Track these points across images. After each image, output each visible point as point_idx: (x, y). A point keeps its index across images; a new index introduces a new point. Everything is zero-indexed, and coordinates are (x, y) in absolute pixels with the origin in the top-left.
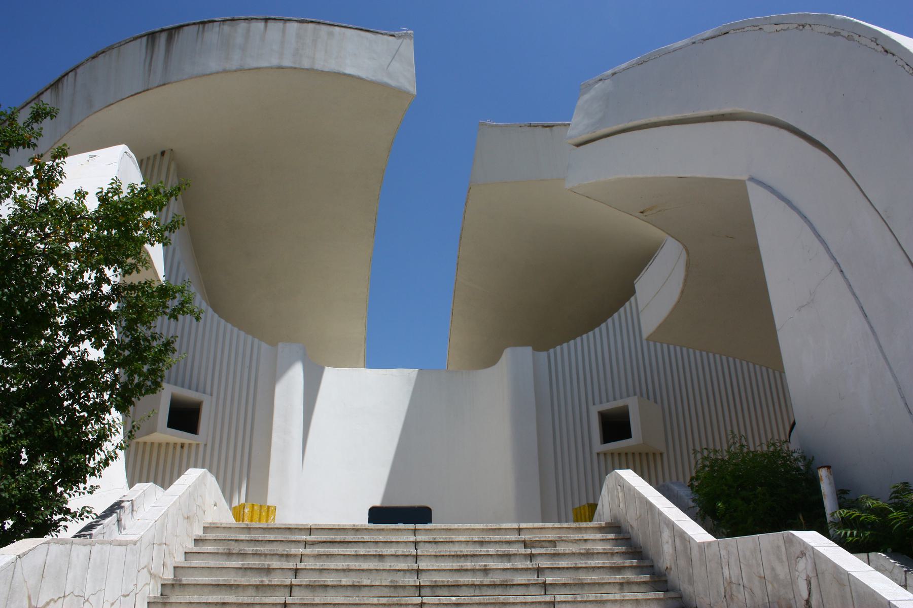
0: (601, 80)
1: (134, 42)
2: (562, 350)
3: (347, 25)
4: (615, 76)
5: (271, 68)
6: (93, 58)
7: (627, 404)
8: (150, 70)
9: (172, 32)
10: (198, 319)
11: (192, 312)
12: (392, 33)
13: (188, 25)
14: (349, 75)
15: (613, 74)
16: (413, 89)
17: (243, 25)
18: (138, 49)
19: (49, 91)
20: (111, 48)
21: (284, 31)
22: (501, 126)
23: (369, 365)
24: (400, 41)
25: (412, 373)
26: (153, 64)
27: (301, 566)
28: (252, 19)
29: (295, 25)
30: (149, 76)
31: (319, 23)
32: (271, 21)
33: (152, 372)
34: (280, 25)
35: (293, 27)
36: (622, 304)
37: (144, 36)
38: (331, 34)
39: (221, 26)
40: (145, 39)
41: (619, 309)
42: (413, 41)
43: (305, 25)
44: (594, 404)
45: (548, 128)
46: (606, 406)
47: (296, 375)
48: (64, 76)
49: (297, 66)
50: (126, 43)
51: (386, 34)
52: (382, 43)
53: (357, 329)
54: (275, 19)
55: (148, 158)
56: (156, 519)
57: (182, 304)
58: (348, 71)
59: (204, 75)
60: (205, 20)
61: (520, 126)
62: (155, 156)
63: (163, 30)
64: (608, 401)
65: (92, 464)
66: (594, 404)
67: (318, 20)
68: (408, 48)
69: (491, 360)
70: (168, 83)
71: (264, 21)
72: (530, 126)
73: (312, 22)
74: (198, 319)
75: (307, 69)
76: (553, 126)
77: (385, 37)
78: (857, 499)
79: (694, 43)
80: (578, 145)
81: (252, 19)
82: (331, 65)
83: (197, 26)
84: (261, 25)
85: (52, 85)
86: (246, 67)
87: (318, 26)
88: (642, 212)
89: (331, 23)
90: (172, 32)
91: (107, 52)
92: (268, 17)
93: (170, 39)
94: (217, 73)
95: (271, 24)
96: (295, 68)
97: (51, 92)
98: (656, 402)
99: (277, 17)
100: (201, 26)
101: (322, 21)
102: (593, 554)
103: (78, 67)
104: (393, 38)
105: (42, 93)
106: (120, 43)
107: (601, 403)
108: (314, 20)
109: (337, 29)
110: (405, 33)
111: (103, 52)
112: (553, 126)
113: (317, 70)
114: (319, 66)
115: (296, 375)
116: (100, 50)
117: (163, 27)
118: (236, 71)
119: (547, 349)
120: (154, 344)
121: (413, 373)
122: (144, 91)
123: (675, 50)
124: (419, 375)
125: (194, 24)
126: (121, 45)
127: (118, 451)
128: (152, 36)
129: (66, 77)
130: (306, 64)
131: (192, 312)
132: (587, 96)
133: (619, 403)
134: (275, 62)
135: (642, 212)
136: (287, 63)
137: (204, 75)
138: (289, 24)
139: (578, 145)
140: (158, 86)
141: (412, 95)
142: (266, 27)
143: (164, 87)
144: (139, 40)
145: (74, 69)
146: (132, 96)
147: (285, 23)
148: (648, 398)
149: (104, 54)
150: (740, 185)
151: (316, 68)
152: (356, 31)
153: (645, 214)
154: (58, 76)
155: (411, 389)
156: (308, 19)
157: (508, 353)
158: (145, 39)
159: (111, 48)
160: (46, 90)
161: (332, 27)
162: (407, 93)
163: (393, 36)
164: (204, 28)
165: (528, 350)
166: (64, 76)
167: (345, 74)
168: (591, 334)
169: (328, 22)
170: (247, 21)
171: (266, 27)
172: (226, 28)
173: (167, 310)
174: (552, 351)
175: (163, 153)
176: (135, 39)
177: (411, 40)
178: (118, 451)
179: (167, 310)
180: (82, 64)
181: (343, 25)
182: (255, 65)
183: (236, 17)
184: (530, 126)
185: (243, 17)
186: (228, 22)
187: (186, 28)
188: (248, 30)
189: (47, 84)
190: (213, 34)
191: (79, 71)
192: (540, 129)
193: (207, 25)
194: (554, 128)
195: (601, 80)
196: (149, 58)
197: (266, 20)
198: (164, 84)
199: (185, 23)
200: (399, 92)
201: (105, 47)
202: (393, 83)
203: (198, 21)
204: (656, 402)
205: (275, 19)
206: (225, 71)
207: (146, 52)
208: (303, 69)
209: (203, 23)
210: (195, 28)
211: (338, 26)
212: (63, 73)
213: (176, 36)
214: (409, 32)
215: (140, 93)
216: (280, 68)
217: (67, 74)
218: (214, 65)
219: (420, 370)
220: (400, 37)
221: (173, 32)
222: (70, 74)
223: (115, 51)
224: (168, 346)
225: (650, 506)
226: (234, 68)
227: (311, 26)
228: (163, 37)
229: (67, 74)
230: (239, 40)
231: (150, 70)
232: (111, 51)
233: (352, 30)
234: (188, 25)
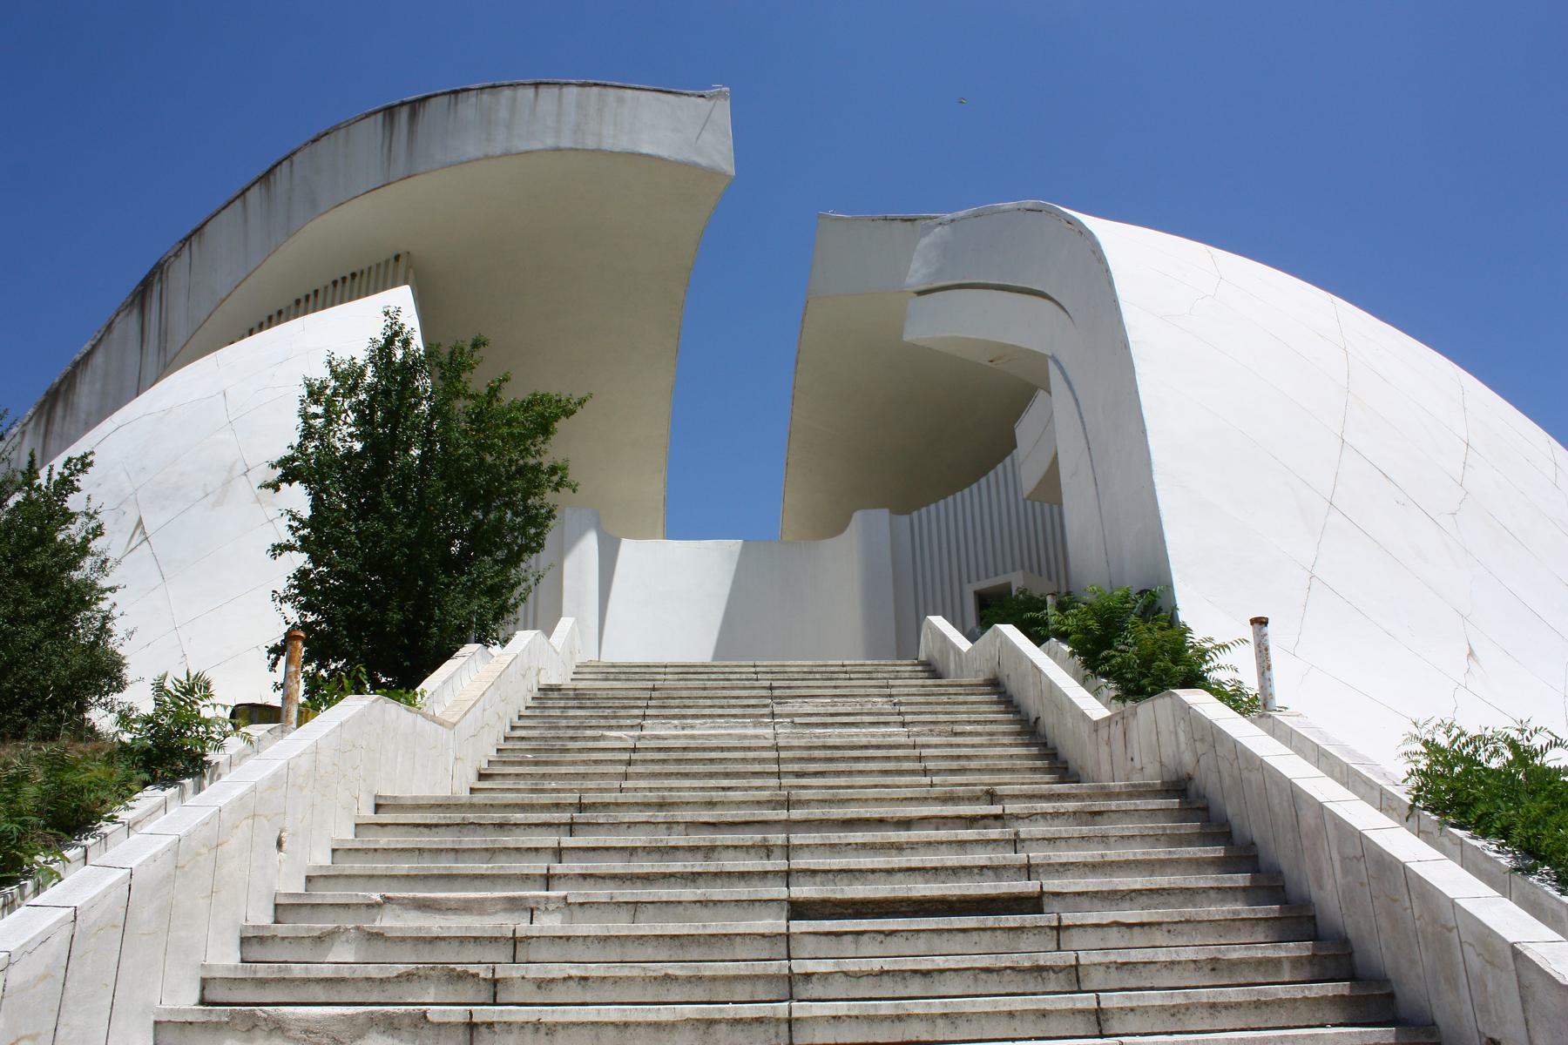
0: (940, 224)
1: (367, 120)
2: (920, 517)
3: (642, 86)
4: (954, 223)
5: (546, 150)
6: (314, 141)
7: (1009, 581)
8: (389, 159)
9: (416, 105)
10: (574, 491)
11: (569, 486)
12: (701, 92)
13: (436, 95)
14: (647, 155)
15: (953, 220)
16: (730, 169)
17: (507, 93)
18: (375, 125)
19: (257, 186)
20: (337, 128)
21: (560, 100)
22: (847, 219)
23: (668, 537)
24: (712, 102)
25: (733, 546)
26: (392, 149)
27: (558, 869)
28: (518, 85)
29: (574, 90)
30: (390, 165)
31: (605, 86)
32: (543, 86)
33: (537, 535)
34: (555, 90)
35: (572, 93)
36: (1001, 459)
37: (379, 111)
38: (621, 100)
39: (479, 96)
40: (380, 116)
41: (1004, 458)
42: (729, 101)
43: (587, 89)
44: (969, 582)
45: (909, 223)
46: (985, 584)
47: (589, 545)
48: (276, 166)
49: (578, 146)
50: (356, 121)
51: (693, 95)
52: (687, 109)
53: (653, 488)
54: (547, 84)
55: (378, 265)
56: (4, 1000)
57: (561, 478)
58: (645, 150)
59: (460, 163)
60: (458, 88)
61: (873, 220)
62: (387, 262)
63: (403, 104)
64: (987, 577)
65: (512, 601)
66: (969, 582)
67: (603, 82)
68: (722, 111)
69: (838, 527)
70: (415, 175)
71: (533, 87)
72: (886, 219)
73: (596, 85)
74: (574, 491)
75: (593, 151)
76: (915, 220)
77: (692, 99)
78: (1181, 650)
79: (1019, 209)
80: (920, 293)
81: (518, 85)
82: (623, 143)
83: (448, 96)
84: (530, 92)
85: (261, 178)
86: (514, 151)
87: (603, 90)
88: (991, 361)
89: (621, 84)
90: (416, 105)
91: (332, 135)
92: (538, 80)
93: (413, 116)
94: (477, 160)
95: (543, 90)
96: (577, 150)
97: (260, 189)
98: (1050, 578)
99: (551, 80)
100: (453, 96)
101: (609, 83)
102: (966, 770)
103: (294, 153)
104: (702, 99)
105: (248, 189)
106: (348, 121)
107: (978, 580)
108: (598, 82)
109: (629, 92)
110: (718, 92)
111: (326, 134)
112: (915, 220)
113: (606, 151)
114: (608, 144)
115: (589, 545)
116: (323, 130)
117: (404, 99)
118: (500, 156)
119: (908, 512)
120: (543, 511)
121: (735, 545)
122: (383, 186)
123: (1004, 211)
124: (744, 548)
125: (443, 94)
126: (350, 125)
127: (304, 670)
128: (390, 112)
129: (279, 167)
130: (591, 143)
131: (569, 486)
132: (926, 241)
133: (1000, 580)
134: (550, 142)
135: (991, 361)
136: (566, 143)
137: (460, 163)
138: (566, 90)
139: (920, 293)
140: (401, 179)
141: (729, 176)
142: (537, 94)
143: (409, 180)
144: (373, 118)
145: (289, 157)
146: (368, 192)
147: (561, 89)
148: (1040, 575)
149: (328, 136)
150: (1044, 357)
151: (603, 148)
152: (654, 93)
153: (994, 363)
154: (269, 166)
155: (734, 567)
156: (590, 81)
157: (858, 516)
158: (380, 116)
159: (337, 128)
160: (254, 184)
161: (623, 90)
162: (723, 174)
163: (703, 96)
164: (456, 98)
165: (883, 515)
166: (276, 166)
167: (641, 155)
168: (966, 491)
169: (617, 84)
170: (512, 87)
171: (537, 94)
172: (486, 97)
173: (551, 484)
174: (915, 514)
175: (397, 258)
176: (368, 115)
177: (726, 100)
178: (304, 670)
179: (551, 484)
180: (299, 150)
181: (637, 86)
182: (524, 146)
183: (497, 83)
184: (885, 219)
185: (506, 82)
186: (487, 90)
187: (433, 100)
188: (514, 100)
189: (255, 177)
190: (468, 107)
191: (296, 158)
192: (898, 224)
193: (460, 95)
194: (917, 222)
195: (940, 224)
196: (387, 141)
197: (537, 85)
198: (409, 177)
199: (433, 93)
200: (711, 173)
201: (329, 127)
202: (703, 162)
203: (449, 90)
204: (1050, 578)
205: (547, 84)
206: (487, 157)
207: (384, 133)
208: (587, 150)
209: (456, 92)
210: (446, 98)
211: (630, 88)
212: (274, 162)
213: (421, 110)
214: (723, 89)
215: (379, 188)
216: (558, 149)
217: (280, 163)
218: (472, 150)
219: (745, 541)
220: (711, 97)
221: (417, 105)
222: (284, 163)
223: (342, 132)
224: (550, 515)
225: (944, 638)
226: (498, 153)
227: (595, 89)
228: (404, 113)
229: (280, 163)
230: (503, 114)
231: (389, 159)
232: (335, 132)
233: (649, 93)
234: (436, 95)
